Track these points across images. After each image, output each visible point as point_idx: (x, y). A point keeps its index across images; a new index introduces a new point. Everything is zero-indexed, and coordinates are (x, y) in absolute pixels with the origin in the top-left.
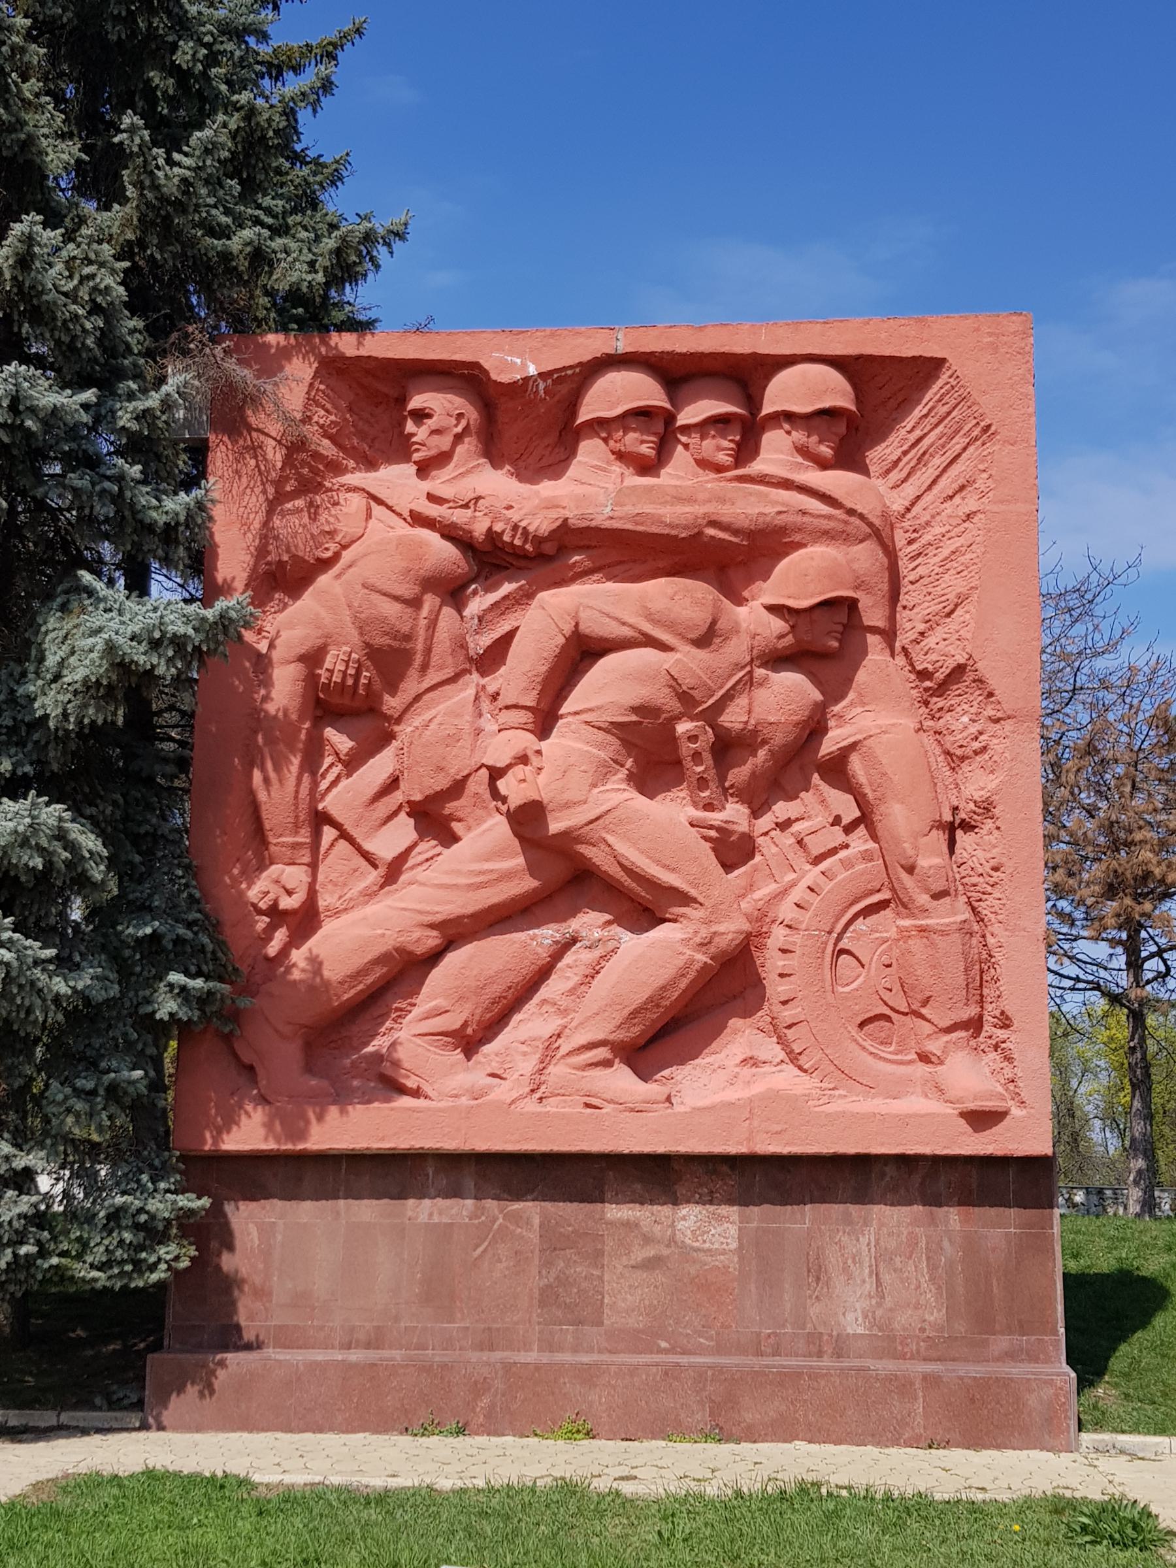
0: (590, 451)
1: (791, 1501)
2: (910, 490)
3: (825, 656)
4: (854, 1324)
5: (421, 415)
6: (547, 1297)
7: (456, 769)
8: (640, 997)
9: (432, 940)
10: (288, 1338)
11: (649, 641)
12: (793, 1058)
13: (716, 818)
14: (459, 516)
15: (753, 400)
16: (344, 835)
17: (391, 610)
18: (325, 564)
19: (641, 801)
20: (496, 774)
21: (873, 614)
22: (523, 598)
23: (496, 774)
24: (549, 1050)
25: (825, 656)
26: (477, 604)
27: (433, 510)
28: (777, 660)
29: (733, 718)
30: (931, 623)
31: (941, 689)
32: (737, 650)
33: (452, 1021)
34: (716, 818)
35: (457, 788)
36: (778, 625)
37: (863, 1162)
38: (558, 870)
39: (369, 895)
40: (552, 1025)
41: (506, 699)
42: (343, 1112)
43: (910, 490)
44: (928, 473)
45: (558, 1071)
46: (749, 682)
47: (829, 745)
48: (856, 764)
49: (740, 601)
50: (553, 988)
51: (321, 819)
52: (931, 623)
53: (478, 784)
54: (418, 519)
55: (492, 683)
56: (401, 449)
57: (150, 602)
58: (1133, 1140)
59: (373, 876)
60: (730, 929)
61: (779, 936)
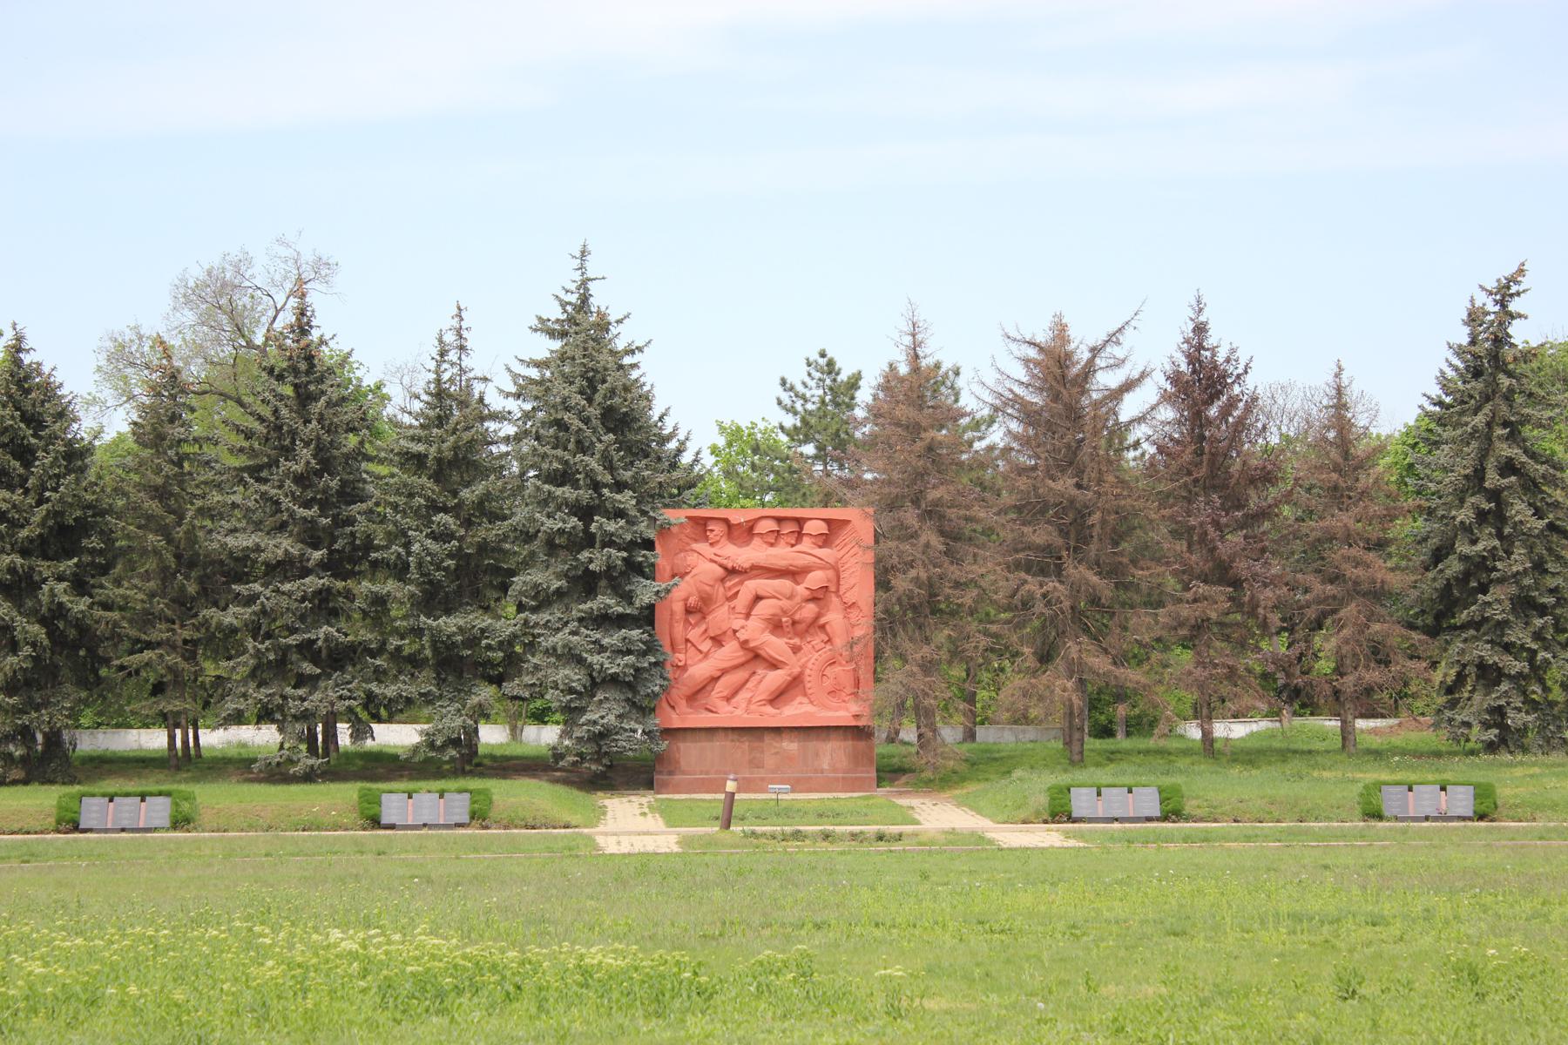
0: (756, 541)
1: (791, 484)
2: (842, 552)
3: (819, 599)
4: (826, 766)
5: (712, 531)
6: (750, 762)
7: (724, 629)
8: (773, 688)
9: (719, 674)
10: (684, 773)
11: (774, 597)
12: (811, 702)
13: (792, 642)
14: (725, 562)
15: (801, 528)
16: (694, 645)
17: (708, 588)
18: (687, 573)
19: (773, 638)
20: (735, 631)
21: (833, 589)
22: (741, 583)
23: (735, 631)
24: (750, 701)
25: (819, 599)
26: (728, 584)
27: (717, 558)
28: (808, 600)
29: (797, 617)
30: (847, 590)
31: (850, 607)
32: (798, 599)
33: (725, 694)
34: (792, 642)
35: (725, 633)
36: (808, 592)
37: (828, 728)
38: (750, 655)
39: (700, 661)
40: (749, 695)
41: (738, 610)
42: (1406, 425)
43: (842, 552)
44: (846, 549)
45: (753, 707)
46: (800, 608)
47: (822, 621)
48: (827, 627)
49: (798, 584)
50: (749, 685)
51: (687, 641)
52: (847, 590)
53: (730, 633)
54: (712, 561)
55: (732, 604)
56: (706, 539)
57: (875, 723)
58: (365, 481)
59: (701, 656)
60: (796, 670)
61: (808, 672)
